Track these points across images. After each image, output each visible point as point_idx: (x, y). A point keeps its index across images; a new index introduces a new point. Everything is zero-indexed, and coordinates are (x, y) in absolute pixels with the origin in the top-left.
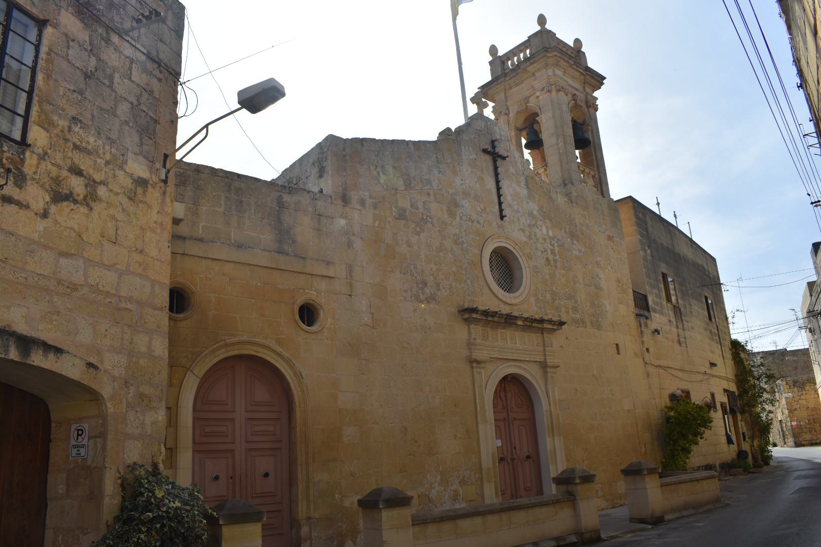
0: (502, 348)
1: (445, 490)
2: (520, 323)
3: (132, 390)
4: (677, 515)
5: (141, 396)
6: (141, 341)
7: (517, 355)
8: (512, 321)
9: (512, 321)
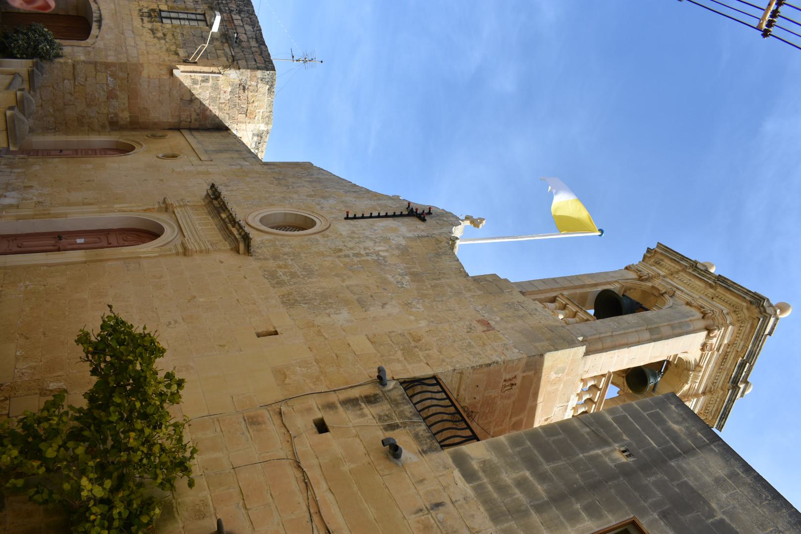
3: (92, 49)
5: (90, 52)
6: (111, 53)
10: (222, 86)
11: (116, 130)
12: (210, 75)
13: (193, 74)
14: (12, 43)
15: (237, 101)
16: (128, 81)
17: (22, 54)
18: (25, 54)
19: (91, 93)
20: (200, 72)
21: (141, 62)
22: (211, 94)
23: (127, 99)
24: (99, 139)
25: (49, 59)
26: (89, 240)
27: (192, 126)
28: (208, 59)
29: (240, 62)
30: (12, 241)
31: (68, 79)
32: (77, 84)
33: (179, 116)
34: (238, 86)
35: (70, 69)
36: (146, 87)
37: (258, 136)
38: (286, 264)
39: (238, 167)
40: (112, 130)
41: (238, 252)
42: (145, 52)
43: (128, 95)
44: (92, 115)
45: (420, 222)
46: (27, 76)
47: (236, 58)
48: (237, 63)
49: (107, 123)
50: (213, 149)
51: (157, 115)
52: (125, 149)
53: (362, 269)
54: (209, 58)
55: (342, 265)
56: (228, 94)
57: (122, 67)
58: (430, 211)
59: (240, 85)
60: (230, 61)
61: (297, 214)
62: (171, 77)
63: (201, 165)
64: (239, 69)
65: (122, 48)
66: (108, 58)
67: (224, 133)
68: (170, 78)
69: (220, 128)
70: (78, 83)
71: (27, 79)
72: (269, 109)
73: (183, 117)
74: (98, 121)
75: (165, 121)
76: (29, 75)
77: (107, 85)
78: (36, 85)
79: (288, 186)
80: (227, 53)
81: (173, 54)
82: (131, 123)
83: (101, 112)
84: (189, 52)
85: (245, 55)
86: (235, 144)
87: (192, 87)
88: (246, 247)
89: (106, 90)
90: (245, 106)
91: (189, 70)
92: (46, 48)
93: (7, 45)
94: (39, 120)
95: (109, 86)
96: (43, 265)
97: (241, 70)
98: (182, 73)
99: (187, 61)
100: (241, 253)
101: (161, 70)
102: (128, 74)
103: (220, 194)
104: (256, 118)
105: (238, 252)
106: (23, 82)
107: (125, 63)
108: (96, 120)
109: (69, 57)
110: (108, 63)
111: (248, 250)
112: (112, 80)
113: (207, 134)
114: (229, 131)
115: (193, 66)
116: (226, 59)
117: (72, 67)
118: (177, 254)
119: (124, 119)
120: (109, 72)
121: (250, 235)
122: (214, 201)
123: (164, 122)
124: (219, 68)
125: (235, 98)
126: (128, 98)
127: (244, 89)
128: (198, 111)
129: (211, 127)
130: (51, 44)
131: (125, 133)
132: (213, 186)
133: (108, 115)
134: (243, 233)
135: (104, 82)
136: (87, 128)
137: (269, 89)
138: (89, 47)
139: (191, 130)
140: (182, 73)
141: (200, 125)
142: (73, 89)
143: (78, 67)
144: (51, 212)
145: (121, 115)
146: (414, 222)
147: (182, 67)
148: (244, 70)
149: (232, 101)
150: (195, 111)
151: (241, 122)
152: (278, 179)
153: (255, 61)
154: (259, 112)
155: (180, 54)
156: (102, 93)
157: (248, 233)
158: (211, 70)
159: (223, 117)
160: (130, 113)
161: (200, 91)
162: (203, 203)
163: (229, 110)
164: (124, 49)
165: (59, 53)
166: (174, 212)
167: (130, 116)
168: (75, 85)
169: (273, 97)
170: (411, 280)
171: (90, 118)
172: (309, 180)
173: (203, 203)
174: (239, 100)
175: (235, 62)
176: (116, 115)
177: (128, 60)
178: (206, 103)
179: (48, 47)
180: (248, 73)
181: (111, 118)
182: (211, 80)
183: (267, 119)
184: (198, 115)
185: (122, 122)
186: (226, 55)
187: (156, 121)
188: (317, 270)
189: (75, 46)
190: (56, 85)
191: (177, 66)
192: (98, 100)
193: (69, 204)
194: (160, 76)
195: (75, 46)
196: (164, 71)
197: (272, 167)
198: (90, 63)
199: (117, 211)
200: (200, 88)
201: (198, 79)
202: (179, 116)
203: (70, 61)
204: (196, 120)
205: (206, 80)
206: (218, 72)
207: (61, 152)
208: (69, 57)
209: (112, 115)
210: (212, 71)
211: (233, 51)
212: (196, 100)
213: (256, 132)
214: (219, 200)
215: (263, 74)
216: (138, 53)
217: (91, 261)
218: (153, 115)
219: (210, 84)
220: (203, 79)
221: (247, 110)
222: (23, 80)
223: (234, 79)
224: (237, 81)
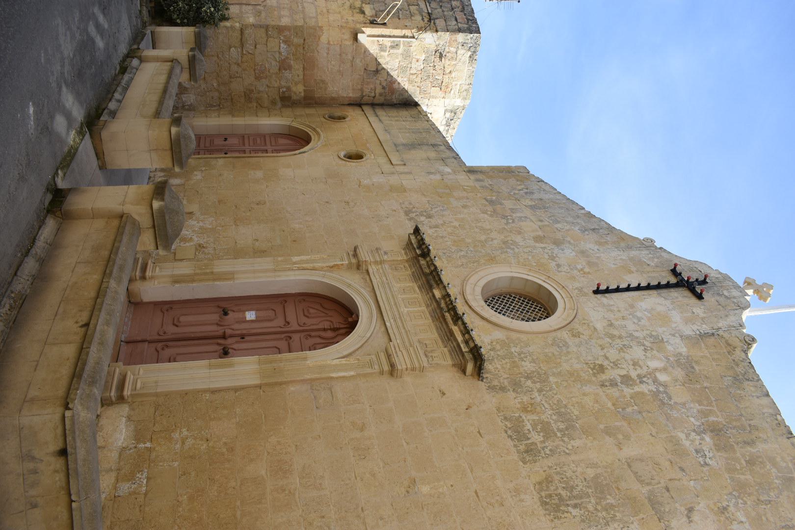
0: (389, 286)
1: (194, 231)
2: (437, 293)
3: (262, 8)
4: (40, 243)
5: (260, 12)
6: (285, 12)
7: (388, 308)
8: (433, 282)
9: (433, 282)
10: (414, 54)
11: (288, 106)
12: (402, 40)
13: (380, 39)
14: (171, 6)
15: (432, 71)
16: (304, 48)
17: (182, 19)
18: (186, 18)
19: (260, 64)
20: (390, 37)
21: (320, 25)
22: (401, 63)
23: (302, 69)
24: (268, 122)
25: (214, 24)
26: (263, 314)
27: (376, 101)
28: (399, 19)
29: (437, 21)
30: (167, 310)
31: (235, 47)
32: (244, 52)
33: (362, 90)
34: (434, 53)
35: (237, 34)
36: (325, 55)
37: (452, 112)
38: (533, 401)
39: (438, 177)
40: (284, 106)
41: (464, 371)
42: (325, 10)
43: (304, 65)
44: (261, 89)
45: (694, 300)
46: (187, 63)
47: (434, 16)
48: (434, 23)
49: (277, 98)
50: (404, 141)
51: (335, 89)
52: (300, 139)
53: (639, 417)
54: (401, 16)
55: (610, 405)
56: (421, 62)
57: (298, 30)
58: (705, 279)
59: (436, 52)
60: (426, 20)
61: (527, 280)
62: (355, 42)
63: (393, 173)
64: (437, 31)
65: (298, 7)
66: (282, 19)
67: (413, 112)
68: (353, 44)
69: (409, 104)
70: (246, 51)
71: (188, 67)
72: (468, 82)
73: (367, 91)
74: (268, 96)
75: (345, 95)
76: (189, 61)
77: (280, 53)
78: (197, 74)
79: (504, 217)
80: (422, 9)
81: (358, 13)
82: (305, 98)
83: (272, 86)
84: (376, 9)
85: (443, 11)
86: (428, 131)
87: (379, 55)
88: (477, 369)
89: (278, 59)
90: (440, 77)
91: (377, 33)
92: (210, 10)
93: (166, 9)
94: (202, 96)
95: (282, 55)
96: (205, 391)
97: (439, 33)
98: (368, 39)
99: (375, 22)
100: (467, 374)
101: (343, 34)
102: (304, 40)
103: (429, 250)
104: (452, 92)
105: (464, 371)
106: (182, 70)
107: (302, 26)
108: (266, 96)
109: (236, 20)
110: (282, 26)
111: (479, 371)
112: (285, 47)
113: (393, 112)
114: (418, 107)
115: (382, 29)
116: (421, 18)
117: (240, 32)
118: (382, 373)
119: (298, 93)
120: (282, 38)
121: (482, 350)
122: (420, 258)
123: (343, 97)
124: (413, 31)
125: (429, 68)
126: (304, 68)
127: (441, 56)
128: (384, 84)
129: (398, 102)
130: (216, 5)
131: (299, 111)
132: (417, 231)
133: (279, 89)
134: (472, 345)
135: (277, 49)
136: (255, 104)
137: (470, 57)
138: (260, 5)
139: (373, 105)
140: (368, 39)
141: (385, 100)
142: (240, 58)
143: (247, 32)
144: (215, 271)
145: (294, 89)
146: (681, 296)
147: (369, 31)
148: (443, 33)
149: (425, 72)
150: (380, 84)
151: (433, 97)
152: (491, 202)
153: (456, 20)
154: (456, 85)
155: (367, 13)
156: (274, 63)
157: (479, 345)
158: (403, 33)
159: (413, 91)
160: (305, 86)
161: (388, 59)
162: (405, 258)
163: (421, 82)
164: (300, 7)
165: (225, 15)
166: (367, 271)
167: (305, 91)
168: (243, 54)
169: (475, 66)
170: (715, 445)
171: (259, 92)
172: (530, 203)
173: (405, 258)
174: (434, 70)
175: (432, 21)
176: (289, 89)
177: (305, 22)
178: (394, 74)
179: (212, 9)
180: (447, 36)
181: (283, 92)
182: (402, 46)
183: (465, 93)
184: (384, 88)
185: (294, 97)
186: (420, 12)
187: (333, 95)
188: (578, 418)
189: (244, 4)
190: (221, 53)
191: (363, 29)
192: (269, 71)
193: (238, 253)
194: (341, 42)
195: (244, 4)
196: (347, 36)
197: (480, 176)
198: (261, 26)
199: (296, 268)
200: (388, 55)
201: (387, 44)
202: (362, 90)
203: (237, 25)
204: (381, 95)
205: (395, 46)
206: (412, 35)
207: (225, 141)
208: (236, 20)
209: (285, 90)
210: (405, 35)
211: (430, 6)
212: (383, 71)
213: (449, 108)
214: (428, 259)
215: (465, 37)
216: (317, 12)
217: (266, 384)
218: (331, 89)
219: (401, 50)
220: (392, 44)
221: (442, 82)
222: (182, 68)
223: (430, 44)
224: (433, 48)
